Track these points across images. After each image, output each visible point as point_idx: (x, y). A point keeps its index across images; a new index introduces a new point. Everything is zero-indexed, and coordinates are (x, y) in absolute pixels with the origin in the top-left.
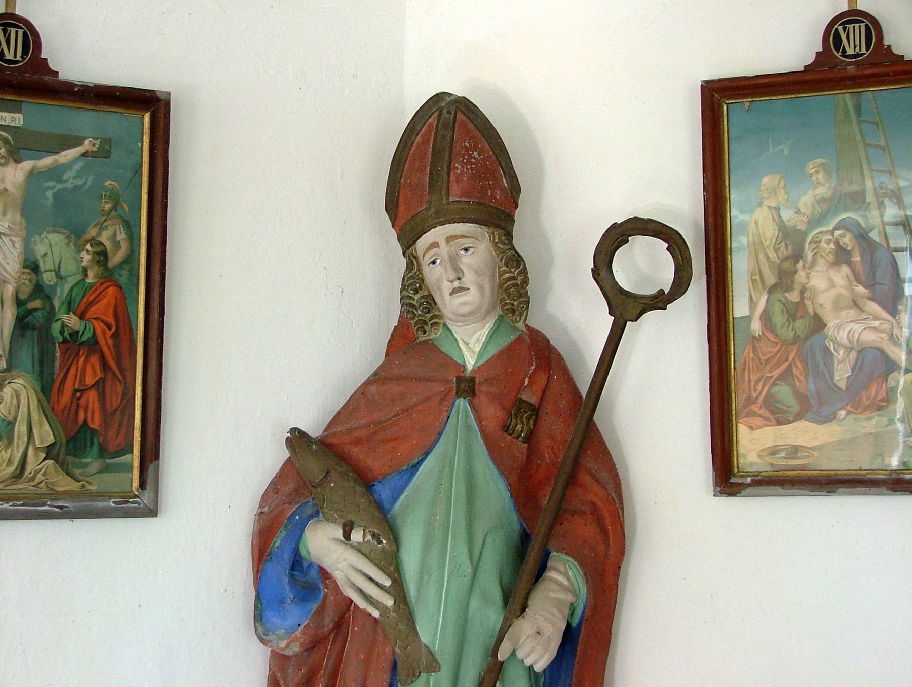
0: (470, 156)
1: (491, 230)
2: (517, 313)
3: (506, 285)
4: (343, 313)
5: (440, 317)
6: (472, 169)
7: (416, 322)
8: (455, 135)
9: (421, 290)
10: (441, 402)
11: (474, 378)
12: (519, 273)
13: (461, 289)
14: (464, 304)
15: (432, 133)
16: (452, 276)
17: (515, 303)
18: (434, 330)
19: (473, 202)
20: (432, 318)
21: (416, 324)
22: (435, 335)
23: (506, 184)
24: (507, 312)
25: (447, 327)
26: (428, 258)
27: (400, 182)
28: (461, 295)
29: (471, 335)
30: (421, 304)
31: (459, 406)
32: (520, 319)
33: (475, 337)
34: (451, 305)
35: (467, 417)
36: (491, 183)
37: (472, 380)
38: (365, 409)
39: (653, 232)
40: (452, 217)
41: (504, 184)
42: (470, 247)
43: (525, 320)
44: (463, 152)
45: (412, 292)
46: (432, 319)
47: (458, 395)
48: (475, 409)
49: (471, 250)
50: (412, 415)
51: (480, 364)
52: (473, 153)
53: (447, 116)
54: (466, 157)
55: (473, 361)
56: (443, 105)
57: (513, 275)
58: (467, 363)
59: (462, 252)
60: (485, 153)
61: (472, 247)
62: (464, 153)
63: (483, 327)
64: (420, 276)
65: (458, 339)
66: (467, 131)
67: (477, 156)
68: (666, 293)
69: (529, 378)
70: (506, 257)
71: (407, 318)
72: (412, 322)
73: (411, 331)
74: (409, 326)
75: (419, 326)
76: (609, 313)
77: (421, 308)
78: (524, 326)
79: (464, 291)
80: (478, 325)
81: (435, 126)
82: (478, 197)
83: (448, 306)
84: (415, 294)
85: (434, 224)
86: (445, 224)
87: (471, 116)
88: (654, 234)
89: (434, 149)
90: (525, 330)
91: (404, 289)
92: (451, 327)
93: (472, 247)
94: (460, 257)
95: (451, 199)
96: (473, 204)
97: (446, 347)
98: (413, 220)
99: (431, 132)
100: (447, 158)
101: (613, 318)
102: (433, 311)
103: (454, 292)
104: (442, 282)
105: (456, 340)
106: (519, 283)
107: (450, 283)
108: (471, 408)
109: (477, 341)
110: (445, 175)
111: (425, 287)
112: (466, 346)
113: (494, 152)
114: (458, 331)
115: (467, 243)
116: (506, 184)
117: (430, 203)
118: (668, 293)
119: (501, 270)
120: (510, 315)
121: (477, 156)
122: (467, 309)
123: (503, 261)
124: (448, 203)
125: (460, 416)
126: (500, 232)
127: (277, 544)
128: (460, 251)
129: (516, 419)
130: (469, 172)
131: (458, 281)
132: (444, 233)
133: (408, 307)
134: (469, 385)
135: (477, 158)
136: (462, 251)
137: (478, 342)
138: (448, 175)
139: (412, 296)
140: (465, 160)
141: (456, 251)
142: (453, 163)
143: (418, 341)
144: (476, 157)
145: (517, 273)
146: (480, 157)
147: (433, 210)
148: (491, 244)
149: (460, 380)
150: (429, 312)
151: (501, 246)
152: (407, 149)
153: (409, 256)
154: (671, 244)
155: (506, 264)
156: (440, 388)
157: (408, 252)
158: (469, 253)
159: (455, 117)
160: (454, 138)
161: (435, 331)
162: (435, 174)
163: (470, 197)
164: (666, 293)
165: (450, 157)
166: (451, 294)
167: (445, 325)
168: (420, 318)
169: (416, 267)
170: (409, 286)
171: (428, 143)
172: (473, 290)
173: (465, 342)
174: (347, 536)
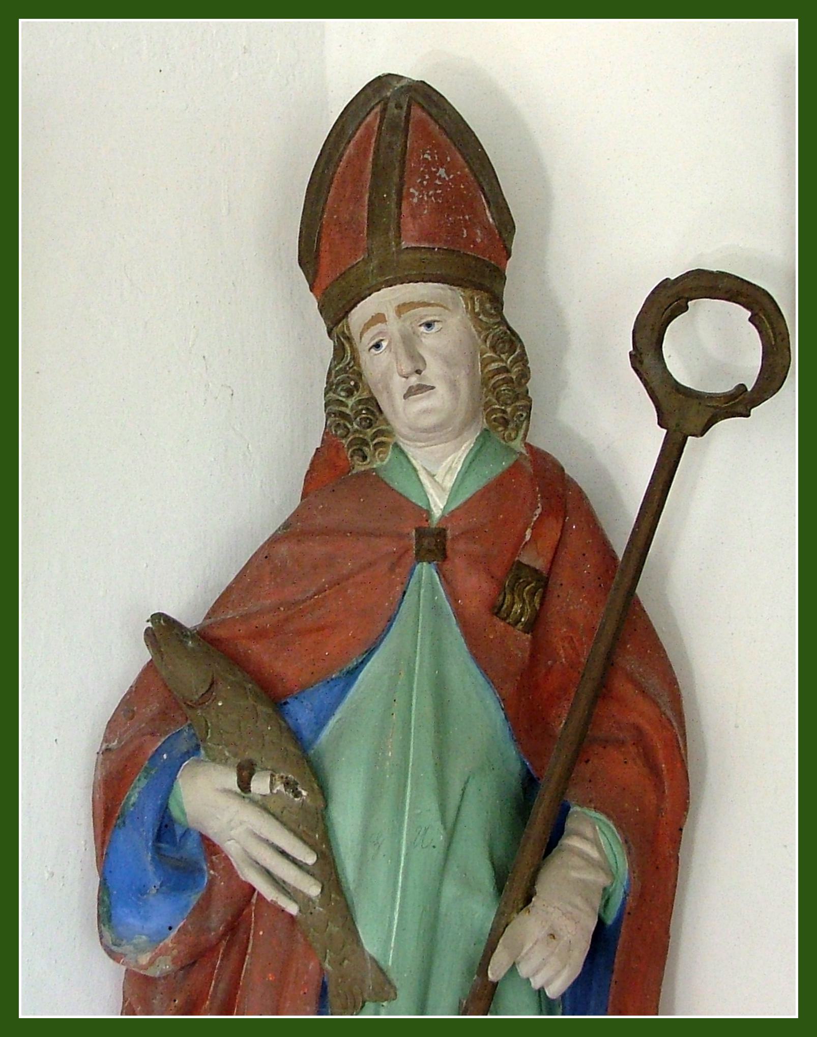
0: (433, 175)
1: (469, 292)
2: (511, 425)
3: (493, 381)
4: (234, 429)
5: (389, 433)
6: (436, 196)
7: (350, 442)
8: (408, 142)
9: (358, 390)
10: (392, 569)
11: (445, 530)
12: (515, 362)
14: (426, 411)
16: (407, 367)
17: (509, 410)
18: (379, 454)
19: (438, 248)
20: (375, 435)
21: (351, 444)
22: (381, 462)
23: (491, 220)
26: (368, 339)
27: (321, 218)
28: (421, 399)
29: (439, 461)
30: (358, 413)
31: (420, 576)
32: (517, 435)
33: (444, 464)
34: (406, 415)
35: (434, 591)
36: (467, 217)
37: (441, 533)
38: (270, 581)
39: (727, 292)
42: (435, 321)
43: (525, 435)
44: (422, 169)
45: (343, 394)
46: (376, 436)
47: (419, 558)
48: (446, 580)
49: (437, 326)
50: (346, 591)
52: (438, 169)
53: (396, 111)
54: (427, 177)
55: (442, 503)
57: (504, 365)
58: (432, 506)
59: (423, 329)
62: (423, 171)
65: (418, 467)
67: (444, 175)
68: (749, 390)
69: (532, 529)
70: (493, 336)
72: (344, 441)
74: (338, 448)
75: (355, 447)
76: (659, 424)
77: (358, 419)
78: (523, 445)
80: (449, 445)
81: (376, 128)
82: (446, 241)
84: (347, 397)
87: (434, 111)
89: (375, 164)
90: (524, 452)
91: (331, 390)
94: (418, 336)
95: (404, 245)
97: (399, 482)
99: (370, 138)
100: (396, 179)
102: (377, 425)
103: (410, 393)
104: (391, 378)
106: (514, 377)
108: (439, 577)
109: (449, 471)
110: (393, 206)
113: (471, 169)
114: (419, 456)
115: (429, 314)
116: (491, 220)
117: (369, 251)
118: (752, 391)
119: (485, 356)
121: (444, 175)
123: (488, 343)
124: (400, 251)
125: (422, 591)
127: (133, 799)
129: (513, 594)
131: (418, 375)
133: (337, 419)
135: (445, 178)
137: (450, 472)
138: (399, 206)
139: (344, 399)
140: (425, 183)
141: (412, 328)
142: (406, 187)
143: (354, 472)
144: (443, 176)
145: (511, 362)
146: (449, 176)
149: (421, 533)
150: (370, 426)
151: (484, 319)
152: (332, 166)
153: (338, 337)
155: (493, 348)
156: (389, 546)
157: (337, 330)
158: (433, 331)
160: (406, 147)
161: (381, 456)
163: (434, 241)
164: (749, 390)
165: (401, 177)
166: (405, 397)
167: (396, 445)
168: (357, 435)
170: (338, 384)
171: (366, 156)
172: (441, 389)
174: (244, 785)
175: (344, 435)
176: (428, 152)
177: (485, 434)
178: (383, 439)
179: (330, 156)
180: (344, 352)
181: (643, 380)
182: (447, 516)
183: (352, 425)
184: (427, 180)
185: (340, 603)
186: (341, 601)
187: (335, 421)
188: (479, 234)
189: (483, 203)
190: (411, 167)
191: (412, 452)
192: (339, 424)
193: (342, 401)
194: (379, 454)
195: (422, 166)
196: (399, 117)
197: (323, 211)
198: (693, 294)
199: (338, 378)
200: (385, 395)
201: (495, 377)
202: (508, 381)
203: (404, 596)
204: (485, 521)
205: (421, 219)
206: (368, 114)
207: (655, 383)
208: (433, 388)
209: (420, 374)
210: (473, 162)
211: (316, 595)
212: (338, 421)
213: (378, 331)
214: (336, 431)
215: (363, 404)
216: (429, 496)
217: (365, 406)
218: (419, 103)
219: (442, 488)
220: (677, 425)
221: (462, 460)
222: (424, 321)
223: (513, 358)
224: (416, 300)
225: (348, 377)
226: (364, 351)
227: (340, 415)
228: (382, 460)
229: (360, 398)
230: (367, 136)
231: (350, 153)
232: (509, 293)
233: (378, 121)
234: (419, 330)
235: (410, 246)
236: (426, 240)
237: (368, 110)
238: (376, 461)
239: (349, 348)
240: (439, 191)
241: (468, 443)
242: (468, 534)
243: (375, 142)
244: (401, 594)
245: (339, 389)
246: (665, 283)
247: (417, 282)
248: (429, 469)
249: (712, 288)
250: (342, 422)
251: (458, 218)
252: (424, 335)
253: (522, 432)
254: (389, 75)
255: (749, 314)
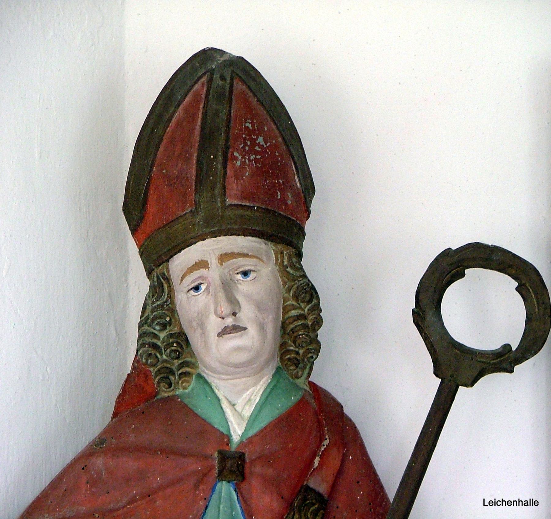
0: (253, 142)
1: (280, 247)
2: (301, 365)
3: (292, 326)
4: (36, 352)
5: (193, 365)
6: (257, 161)
7: (159, 370)
8: (232, 111)
9: (170, 325)
10: (196, 487)
11: (243, 454)
12: (311, 310)
13: (236, 329)
14: (238, 349)
15: (199, 104)
16: (225, 309)
17: (301, 351)
18: (182, 383)
19: (257, 207)
20: (182, 365)
21: (159, 372)
23: (298, 185)
24: (289, 363)
25: (205, 379)
26: (190, 281)
27: (151, 171)
28: (234, 337)
29: (240, 393)
30: (169, 345)
31: (220, 492)
32: (303, 374)
33: (244, 396)
34: (218, 350)
35: (232, 508)
36: (281, 181)
37: (241, 456)
38: (86, 491)
39: (500, 264)
40: (229, 226)
41: (296, 183)
42: (251, 271)
43: (309, 375)
44: (244, 136)
45: (158, 328)
46: (183, 367)
47: (221, 476)
48: (243, 498)
49: (252, 275)
50: (155, 502)
51: (251, 433)
52: (257, 138)
53: (221, 83)
54: (249, 143)
55: (241, 430)
56: (214, 66)
57: (302, 312)
58: (232, 432)
59: (239, 277)
60: (273, 140)
61: (253, 271)
62: (245, 138)
63: (255, 384)
64: (170, 305)
65: (221, 397)
66: (248, 107)
67: (262, 143)
68: (514, 349)
69: (320, 458)
70: (297, 287)
71: (146, 363)
72: (152, 369)
73: (150, 382)
74: (147, 376)
75: (162, 376)
76: (434, 373)
77: (168, 351)
78: (307, 383)
79: (240, 331)
80: (249, 380)
81: (203, 96)
82: (264, 202)
83: (214, 350)
84: (161, 330)
85: (201, 235)
86: (219, 236)
87: (252, 84)
88: (501, 267)
89: (202, 129)
90: (308, 389)
91: (146, 323)
92: (210, 380)
93: (253, 271)
94: (235, 283)
95: (228, 201)
96: (257, 210)
98: (170, 227)
99: (198, 102)
100: (222, 142)
101: (439, 380)
102: (183, 356)
103: (225, 331)
104: (207, 317)
105: (218, 399)
106: (310, 323)
107: (220, 319)
108: (237, 496)
109: (248, 402)
110: (219, 166)
111: (175, 322)
112: (231, 407)
113: (284, 139)
115: (246, 264)
116: (298, 185)
117: (197, 205)
118: (516, 349)
119: (287, 304)
120: (292, 368)
121: (262, 143)
122: (242, 357)
123: (292, 292)
124: (225, 207)
125: (222, 506)
126: (290, 252)
128: (235, 275)
129: (300, 514)
130: (253, 165)
131: (234, 317)
132: (216, 249)
133: (150, 349)
134: (238, 463)
135: (263, 145)
136: (240, 275)
137: (249, 403)
138: (225, 168)
139: (157, 333)
140: (247, 148)
141: (230, 275)
142: (231, 150)
143: (159, 397)
144: (261, 144)
145: (308, 310)
146: (266, 145)
147: (202, 215)
148: (277, 268)
149: (224, 456)
150: (178, 358)
151: (291, 272)
152: (161, 127)
153: (158, 278)
154: (523, 282)
155: (296, 297)
156: (194, 466)
157: (157, 271)
158: (249, 279)
159: (231, 86)
160: (231, 116)
161: (184, 384)
162: (205, 164)
163: (254, 201)
164: (514, 349)
165: (227, 141)
166: (220, 335)
167: (200, 376)
168: (165, 365)
169: (166, 294)
170: (153, 320)
171: (194, 120)
172: (252, 330)
173: (230, 402)
175: (154, 364)
176: (249, 121)
177: (278, 371)
178: (188, 369)
179: (160, 116)
180: (163, 289)
181: (423, 334)
182: (246, 441)
183: (161, 354)
184: (249, 146)
185: (148, 513)
186: (149, 511)
187: (148, 351)
188: (290, 197)
189: (293, 170)
190: (234, 134)
191: (216, 383)
192: (150, 353)
193: (155, 334)
194: (182, 383)
195: (244, 134)
196: (223, 88)
197: (152, 165)
198: (470, 264)
199: (154, 314)
200: (199, 331)
201: (294, 323)
202: (305, 326)
203: (206, 510)
204: (277, 448)
205: (243, 179)
206: (196, 83)
207: (434, 338)
208: (245, 329)
209: (235, 316)
210: (285, 133)
211: (128, 504)
212: (151, 351)
213: (199, 276)
214: (147, 360)
215: (175, 338)
216: (230, 424)
217: (176, 340)
218: (241, 77)
219: (241, 417)
220: (452, 376)
221: (261, 393)
222: (241, 270)
223: (310, 307)
224: (236, 251)
225: (164, 313)
226: (182, 291)
227: (153, 345)
228: (185, 388)
229: (171, 332)
230: (196, 101)
231: (179, 115)
232: (307, 247)
233: (205, 90)
234: (235, 277)
235: (233, 203)
236: (245, 198)
237: (196, 78)
238: (179, 389)
239: (166, 288)
240: (258, 157)
241: (264, 380)
242: (263, 458)
243: (204, 107)
244: (204, 508)
245: (156, 323)
246: (447, 252)
247: (239, 235)
248: (230, 399)
249: (487, 259)
250: (153, 352)
251: (274, 181)
252: (241, 282)
253: (307, 371)
254: (213, 49)
255: (516, 284)
